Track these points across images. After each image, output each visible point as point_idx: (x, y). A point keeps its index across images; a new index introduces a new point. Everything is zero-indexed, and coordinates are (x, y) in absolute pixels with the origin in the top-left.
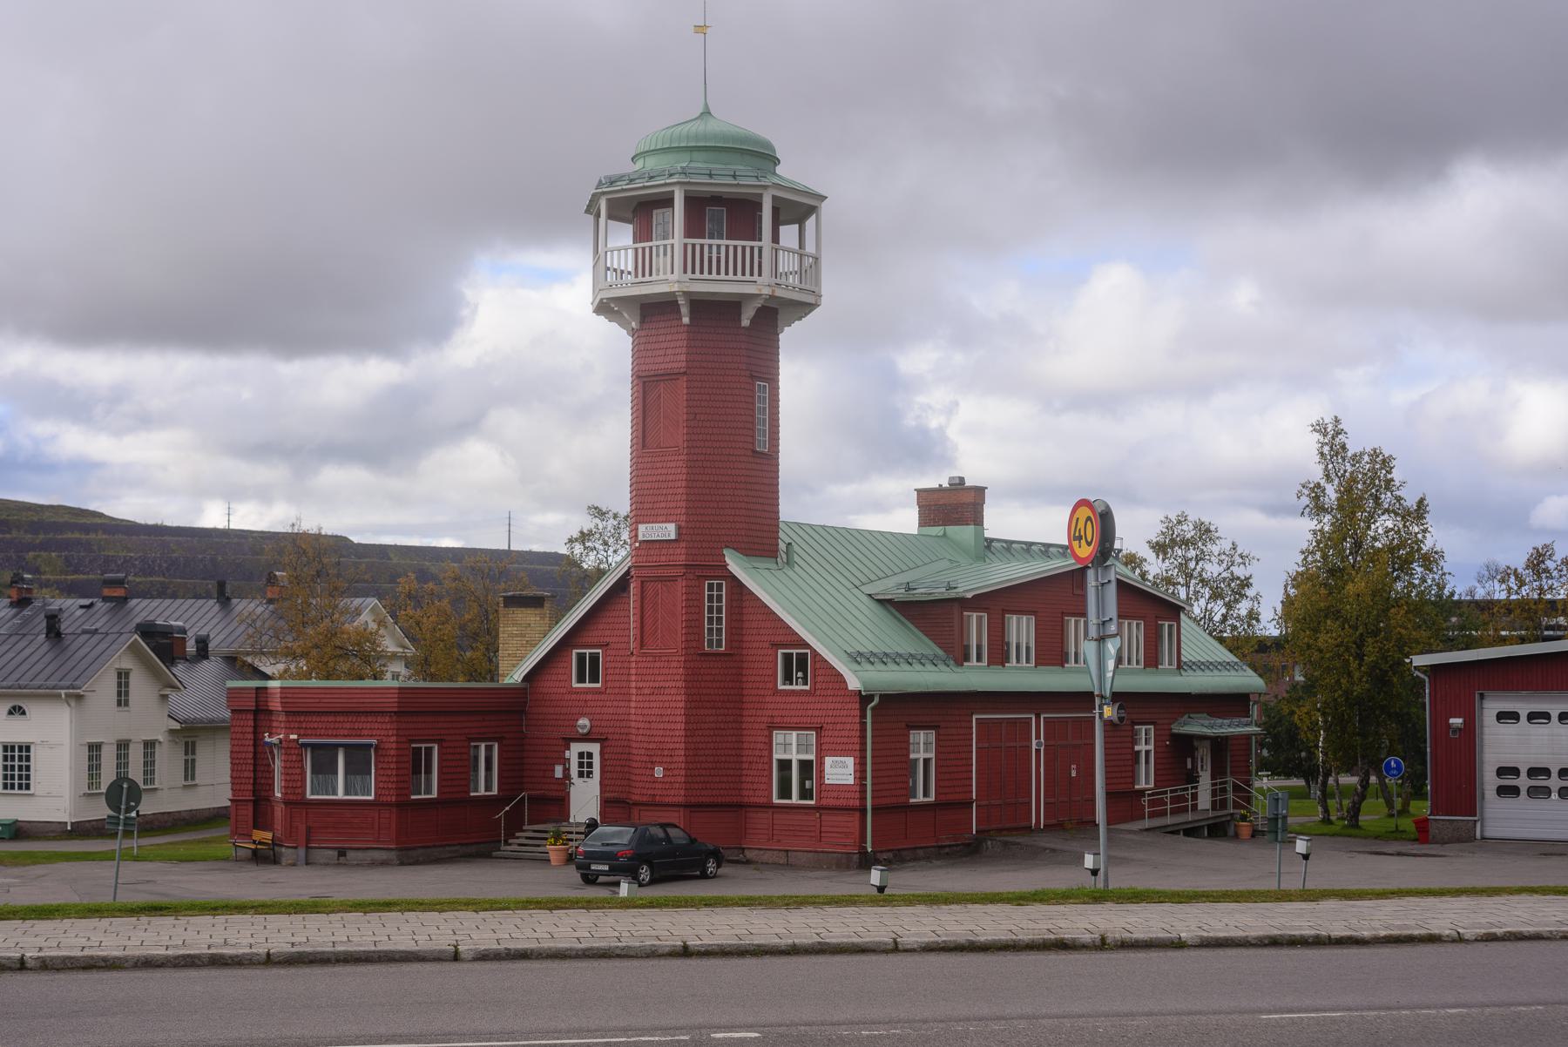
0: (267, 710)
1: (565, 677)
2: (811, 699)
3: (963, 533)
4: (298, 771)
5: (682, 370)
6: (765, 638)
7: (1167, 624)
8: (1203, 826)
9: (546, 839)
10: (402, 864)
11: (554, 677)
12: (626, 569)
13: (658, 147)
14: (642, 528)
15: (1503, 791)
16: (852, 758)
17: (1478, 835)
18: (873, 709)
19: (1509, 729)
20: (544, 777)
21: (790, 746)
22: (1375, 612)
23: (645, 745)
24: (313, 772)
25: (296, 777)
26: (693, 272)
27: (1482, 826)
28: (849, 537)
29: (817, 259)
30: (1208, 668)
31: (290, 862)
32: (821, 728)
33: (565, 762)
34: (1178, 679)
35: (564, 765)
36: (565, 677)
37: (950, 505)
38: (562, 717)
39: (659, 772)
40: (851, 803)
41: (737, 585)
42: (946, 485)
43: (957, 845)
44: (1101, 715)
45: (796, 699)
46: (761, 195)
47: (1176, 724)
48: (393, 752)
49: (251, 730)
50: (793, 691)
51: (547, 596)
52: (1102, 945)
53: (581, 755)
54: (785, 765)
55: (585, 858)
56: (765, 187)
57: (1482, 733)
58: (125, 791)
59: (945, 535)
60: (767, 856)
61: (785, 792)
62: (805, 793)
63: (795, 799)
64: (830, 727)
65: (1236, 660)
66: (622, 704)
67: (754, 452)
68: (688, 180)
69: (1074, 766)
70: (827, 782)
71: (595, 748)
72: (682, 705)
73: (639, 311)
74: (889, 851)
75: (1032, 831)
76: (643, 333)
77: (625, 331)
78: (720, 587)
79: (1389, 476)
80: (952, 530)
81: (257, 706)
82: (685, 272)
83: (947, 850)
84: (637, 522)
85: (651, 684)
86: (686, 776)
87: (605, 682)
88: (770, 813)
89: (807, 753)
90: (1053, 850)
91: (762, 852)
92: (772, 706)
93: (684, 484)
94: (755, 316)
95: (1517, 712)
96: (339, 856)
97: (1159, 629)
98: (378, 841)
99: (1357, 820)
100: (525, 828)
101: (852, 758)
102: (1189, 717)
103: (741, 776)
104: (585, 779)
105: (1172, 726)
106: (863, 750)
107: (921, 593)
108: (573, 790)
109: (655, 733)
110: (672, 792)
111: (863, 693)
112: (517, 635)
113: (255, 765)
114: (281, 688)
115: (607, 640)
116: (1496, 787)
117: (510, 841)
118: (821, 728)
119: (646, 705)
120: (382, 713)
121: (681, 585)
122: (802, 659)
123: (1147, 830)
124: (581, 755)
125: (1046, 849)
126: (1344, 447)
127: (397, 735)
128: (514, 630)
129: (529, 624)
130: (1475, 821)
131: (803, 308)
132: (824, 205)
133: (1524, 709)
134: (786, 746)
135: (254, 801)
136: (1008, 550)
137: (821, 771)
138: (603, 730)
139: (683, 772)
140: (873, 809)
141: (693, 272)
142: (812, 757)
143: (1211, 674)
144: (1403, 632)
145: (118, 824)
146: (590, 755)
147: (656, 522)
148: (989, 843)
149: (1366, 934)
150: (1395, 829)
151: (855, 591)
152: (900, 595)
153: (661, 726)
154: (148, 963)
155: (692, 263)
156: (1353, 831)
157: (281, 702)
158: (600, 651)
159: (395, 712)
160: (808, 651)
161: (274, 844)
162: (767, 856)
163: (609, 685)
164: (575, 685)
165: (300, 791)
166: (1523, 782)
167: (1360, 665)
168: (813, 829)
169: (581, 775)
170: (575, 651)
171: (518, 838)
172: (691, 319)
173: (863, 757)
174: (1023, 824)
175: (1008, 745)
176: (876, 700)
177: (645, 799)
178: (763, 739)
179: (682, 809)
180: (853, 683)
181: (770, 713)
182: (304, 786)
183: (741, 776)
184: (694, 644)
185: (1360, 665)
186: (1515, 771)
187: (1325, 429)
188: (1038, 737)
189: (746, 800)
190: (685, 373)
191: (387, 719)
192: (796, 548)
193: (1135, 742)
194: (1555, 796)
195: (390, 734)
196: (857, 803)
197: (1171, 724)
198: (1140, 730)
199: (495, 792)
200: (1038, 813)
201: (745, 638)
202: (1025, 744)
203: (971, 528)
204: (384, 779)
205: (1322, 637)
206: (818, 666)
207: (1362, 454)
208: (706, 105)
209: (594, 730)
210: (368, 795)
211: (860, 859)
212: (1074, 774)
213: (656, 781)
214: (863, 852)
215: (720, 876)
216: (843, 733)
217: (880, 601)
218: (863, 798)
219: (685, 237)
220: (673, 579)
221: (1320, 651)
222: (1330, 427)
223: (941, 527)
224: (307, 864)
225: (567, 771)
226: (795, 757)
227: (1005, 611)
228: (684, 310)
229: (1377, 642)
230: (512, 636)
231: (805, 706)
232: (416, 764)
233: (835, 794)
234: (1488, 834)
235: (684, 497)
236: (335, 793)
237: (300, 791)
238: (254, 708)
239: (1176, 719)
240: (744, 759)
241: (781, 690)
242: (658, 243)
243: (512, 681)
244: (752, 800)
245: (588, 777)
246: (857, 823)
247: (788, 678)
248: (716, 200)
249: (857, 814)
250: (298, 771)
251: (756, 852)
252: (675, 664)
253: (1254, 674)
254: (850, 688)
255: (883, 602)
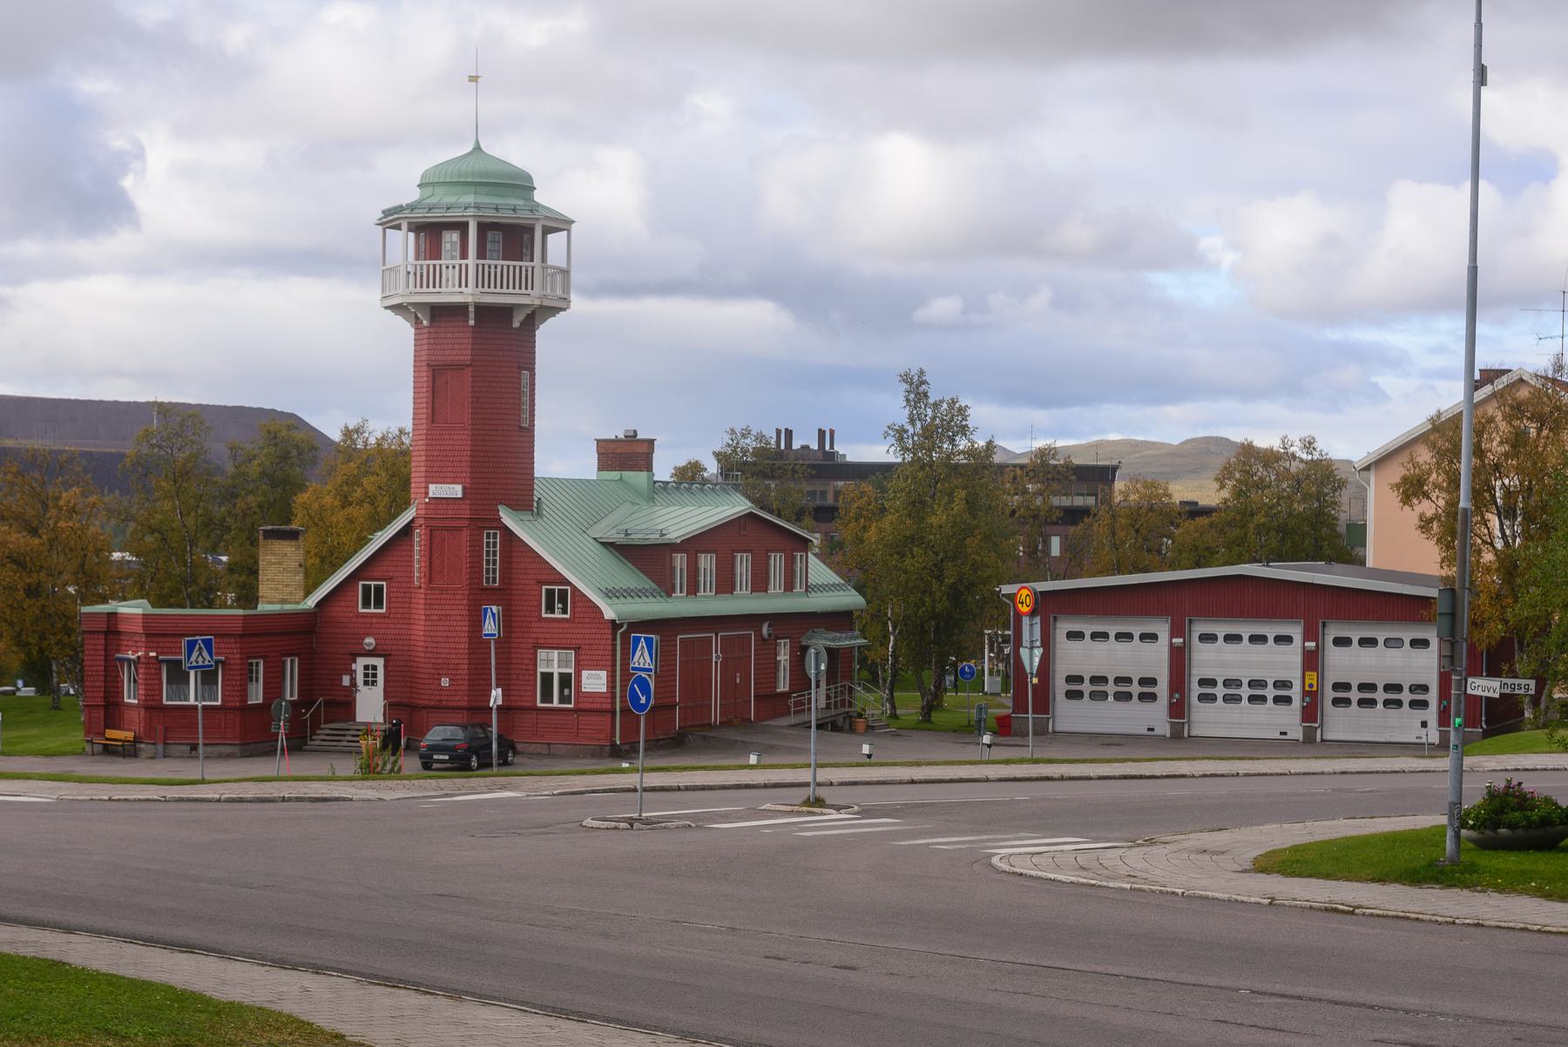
0: (115, 631)
1: (352, 604)
2: (571, 625)
3: (638, 478)
4: (156, 682)
5: (468, 363)
6: (532, 577)
7: (799, 554)
8: (827, 723)
9: (358, 736)
10: (242, 757)
11: (342, 604)
12: (411, 518)
13: (441, 181)
14: (432, 487)
15: (1152, 682)
16: (605, 672)
17: (1186, 735)
18: (621, 633)
19: (1075, 645)
20: (332, 685)
21: (552, 662)
22: (955, 541)
23: (433, 661)
24: (167, 683)
25: (155, 687)
26: (483, 287)
27: (1189, 726)
28: (567, 484)
29: (568, 272)
30: (825, 589)
31: (149, 755)
32: (579, 648)
33: (352, 673)
34: (805, 600)
35: (352, 675)
36: (352, 604)
37: (626, 454)
38: (349, 636)
39: (445, 682)
40: (604, 706)
41: (508, 534)
42: (621, 436)
43: (668, 739)
44: (1031, 682)
45: (558, 625)
46: (534, 224)
47: (804, 637)
48: (237, 667)
49: (102, 647)
50: (554, 619)
51: (302, 531)
52: (1062, 778)
53: (366, 667)
54: (547, 677)
55: (428, 750)
56: (537, 219)
57: (1055, 648)
58: (283, 707)
59: (621, 479)
60: (532, 748)
61: (547, 696)
62: (563, 699)
63: (556, 704)
64: (587, 647)
65: (843, 582)
66: (405, 626)
67: (520, 427)
68: (481, 214)
69: (738, 674)
70: (583, 690)
71: (379, 662)
72: (466, 629)
73: (429, 312)
74: (628, 743)
75: (711, 727)
76: (432, 330)
77: (409, 324)
78: (495, 534)
79: (964, 423)
80: (627, 475)
81: (108, 628)
82: (477, 287)
83: (661, 742)
84: (427, 483)
85: (439, 612)
86: (469, 685)
87: (389, 608)
88: (535, 715)
89: (566, 667)
90: (743, 742)
91: (527, 745)
92: (537, 630)
93: (469, 453)
94: (525, 320)
95: (1131, 633)
96: (191, 749)
97: (794, 557)
98: (225, 739)
99: (930, 716)
100: (323, 726)
101: (605, 672)
102: (813, 631)
103: (510, 684)
104: (370, 687)
105: (802, 639)
106: (614, 666)
107: (636, 538)
108: (359, 697)
109: (442, 651)
110: (458, 698)
111: (618, 622)
112: (275, 563)
113: (105, 676)
114: (143, 615)
115: (391, 574)
116: (1064, 692)
117: (314, 737)
118: (579, 648)
119: (434, 628)
120: (229, 635)
121: (465, 534)
122: (563, 594)
123: (794, 726)
124: (366, 667)
125: (738, 741)
126: (925, 395)
127: (241, 653)
128: (273, 559)
129: (286, 554)
130: (1183, 723)
131: (554, 311)
132: (573, 226)
133: (1088, 628)
134: (549, 662)
135: (105, 706)
136: (665, 489)
137: (579, 682)
138: (387, 648)
139: (467, 682)
140: (621, 711)
141: (483, 287)
142: (571, 670)
143: (821, 595)
144: (977, 558)
145: (279, 729)
146: (375, 668)
147: (444, 483)
148: (690, 737)
149: (1159, 774)
150: (967, 724)
151: (584, 535)
152: (619, 538)
153: (447, 645)
154: (723, 788)
155: (483, 279)
156: (924, 725)
157: (143, 627)
158: (384, 583)
159: (239, 635)
160: (569, 588)
161: (135, 742)
162: (532, 748)
163: (393, 610)
164: (361, 610)
165: (158, 698)
166: (1086, 687)
167: (940, 586)
168: (571, 726)
169: (366, 683)
170: (361, 583)
171: (319, 735)
172: (476, 322)
173: (614, 671)
174: (707, 722)
175: (556, 663)
176: (625, 627)
177: (432, 703)
178: (529, 656)
179: (465, 711)
180: (609, 614)
181: (535, 635)
182: (161, 695)
183: (510, 684)
184: (476, 581)
185: (940, 586)
186: (1080, 679)
187: (911, 379)
188: (716, 652)
189: (513, 704)
190: (470, 365)
191: (232, 640)
192: (543, 499)
193: (776, 655)
194: (1111, 698)
195: (235, 651)
196: (609, 706)
197: (800, 638)
198: (781, 643)
199: (296, 698)
200: (716, 716)
201: (514, 576)
202: (709, 657)
203: (644, 474)
204: (230, 688)
205: (908, 561)
206: (577, 599)
207: (942, 401)
208: (477, 142)
209: (379, 647)
210: (214, 701)
211: (611, 749)
212: (738, 681)
213: (442, 689)
214: (613, 744)
215: (516, 764)
216: (598, 652)
217: (602, 543)
218: (614, 703)
219: (478, 259)
220: (460, 529)
221: (906, 572)
222: (916, 378)
223: (617, 472)
224: (165, 757)
225: (353, 680)
226: (556, 670)
227: (698, 551)
228: (472, 315)
229: (955, 566)
230: (270, 563)
231: (565, 631)
232: (248, 675)
233: (591, 700)
234: (1058, 728)
235: (469, 464)
236: (187, 699)
237: (158, 698)
238: (105, 630)
239: (804, 633)
240: (512, 672)
241: (545, 618)
242: (448, 262)
243: (306, 607)
244: (519, 704)
245: (373, 685)
246: (609, 719)
247: (551, 609)
248: (495, 226)
249: (609, 715)
250: (156, 682)
251: (523, 745)
252: (460, 597)
253: (857, 594)
254: (606, 618)
255: (608, 545)
